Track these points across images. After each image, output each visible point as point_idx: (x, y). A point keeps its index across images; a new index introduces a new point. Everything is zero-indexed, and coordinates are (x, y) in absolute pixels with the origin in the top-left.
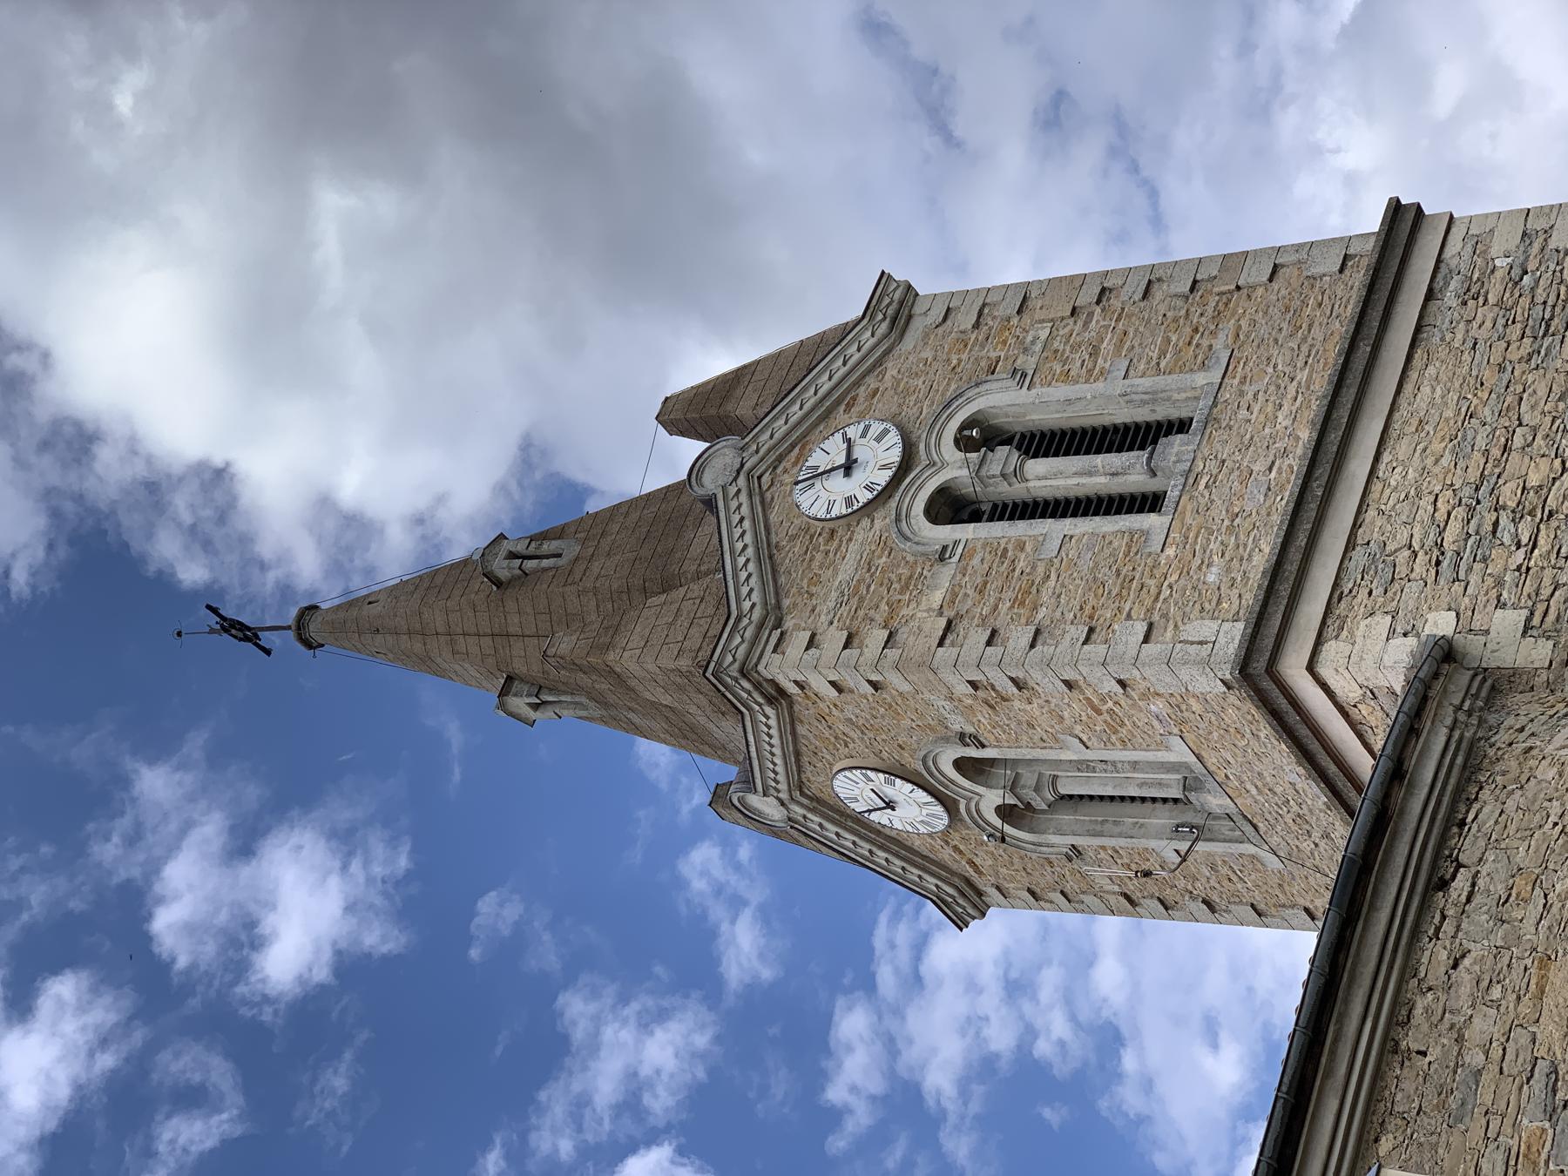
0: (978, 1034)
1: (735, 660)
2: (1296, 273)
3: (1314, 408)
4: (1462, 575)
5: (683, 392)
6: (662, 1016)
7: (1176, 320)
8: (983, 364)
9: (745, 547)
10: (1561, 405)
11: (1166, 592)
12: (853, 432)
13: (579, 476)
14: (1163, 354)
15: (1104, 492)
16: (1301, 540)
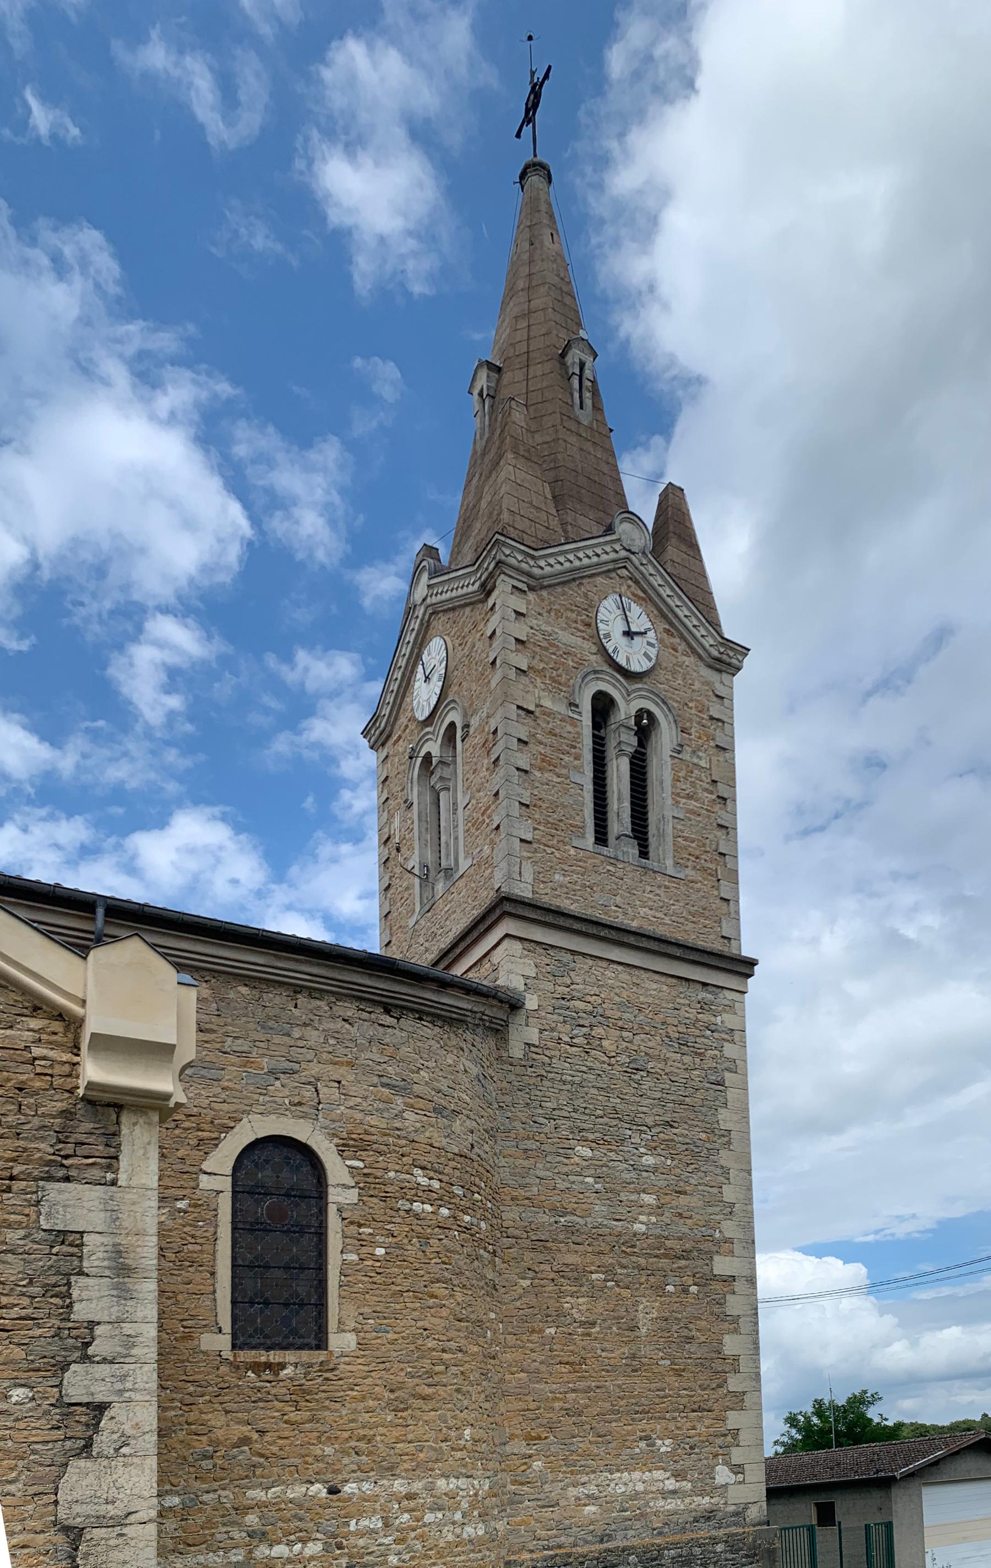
0: (349, 752)
1: (507, 556)
2: (724, 912)
3: (649, 929)
4: (556, 1011)
5: (686, 503)
6: (332, 523)
7: (704, 845)
8: (688, 724)
9: (580, 559)
10: (643, 1054)
11: (549, 851)
12: (651, 634)
13: (679, 429)
14: (686, 839)
15: (609, 808)
16: (577, 926)
